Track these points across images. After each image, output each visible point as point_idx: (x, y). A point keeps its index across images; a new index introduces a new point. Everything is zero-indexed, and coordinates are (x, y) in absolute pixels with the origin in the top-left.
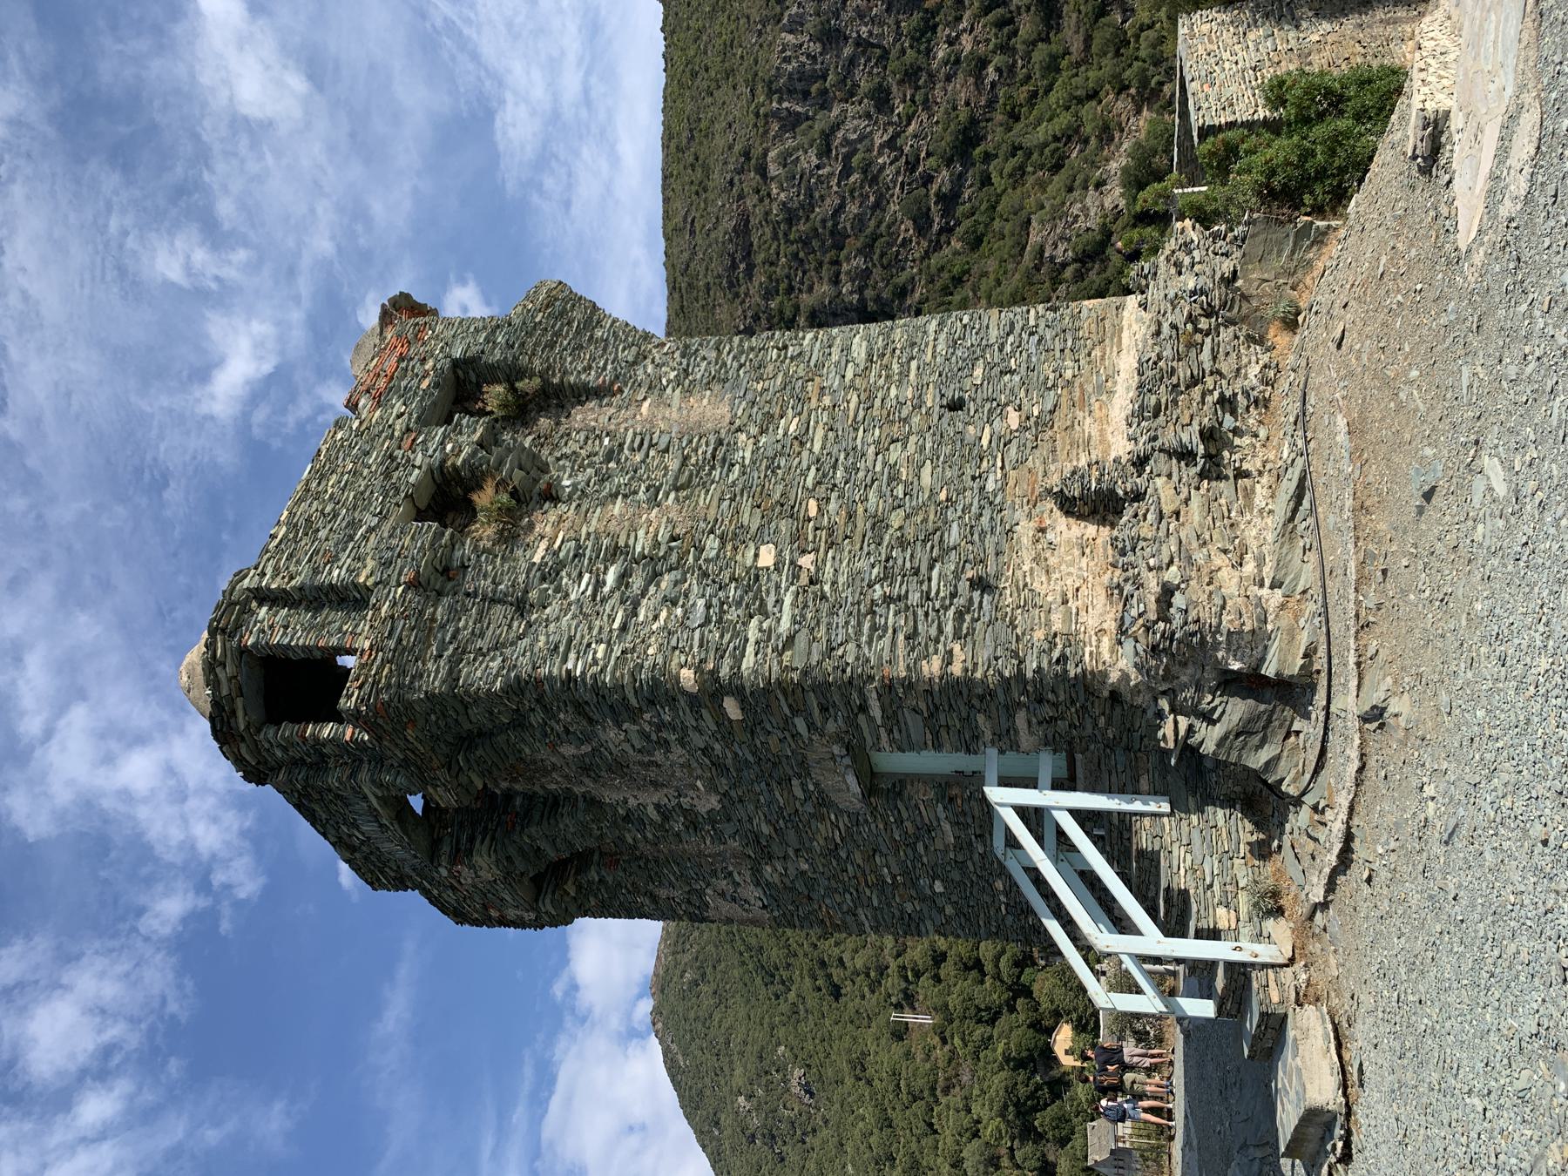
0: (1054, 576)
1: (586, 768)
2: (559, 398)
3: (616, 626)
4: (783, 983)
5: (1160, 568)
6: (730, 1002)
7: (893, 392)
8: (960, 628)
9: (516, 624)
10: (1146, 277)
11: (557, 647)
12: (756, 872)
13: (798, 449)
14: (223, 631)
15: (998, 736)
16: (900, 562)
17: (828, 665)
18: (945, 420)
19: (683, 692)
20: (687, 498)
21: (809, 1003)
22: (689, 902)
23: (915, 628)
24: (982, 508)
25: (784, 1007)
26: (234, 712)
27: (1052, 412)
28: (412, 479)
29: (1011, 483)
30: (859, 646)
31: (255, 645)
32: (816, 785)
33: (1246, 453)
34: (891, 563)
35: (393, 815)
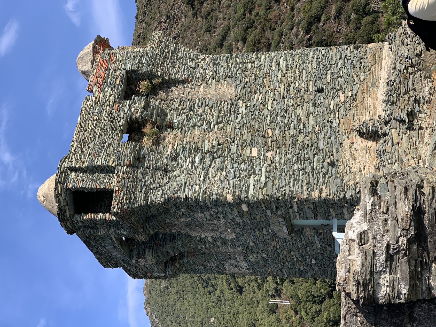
0: (357, 161)
1: (188, 225)
2: (168, 84)
3: (202, 178)
4: (213, 286)
5: (392, 164)
6: (186, 297)
7: (297, 84)
8: (325, 180)
9: (165, 178)
10: (391, 40)
11: (181, 186)
12: (246, 258)
13: (263, 108)
14: (60, 183)
15: (337, 215)
16: (303, 155)
17: (279, 194)
18: (317, 97)
19: (228, 203)
20: (222, 128)
21: (226, 296)
22: (218, 268)
23: (309, 180)
24: (331, 134)
25: (214, 298)
26: (65, 211)
27: (356, 95)
28: (121, 123)
29: (342, 124)
30: (290, 187)
31: (72, 187)
32: (272, 230)
33: (422, 120)
34: (300, 156)
35: (119, 243)
